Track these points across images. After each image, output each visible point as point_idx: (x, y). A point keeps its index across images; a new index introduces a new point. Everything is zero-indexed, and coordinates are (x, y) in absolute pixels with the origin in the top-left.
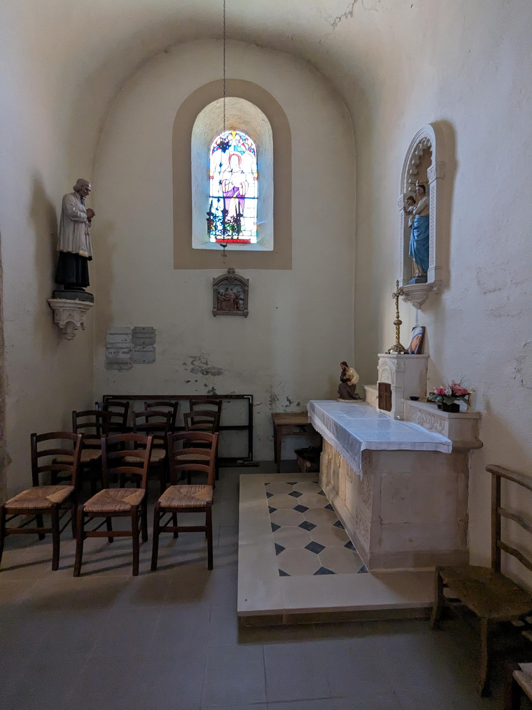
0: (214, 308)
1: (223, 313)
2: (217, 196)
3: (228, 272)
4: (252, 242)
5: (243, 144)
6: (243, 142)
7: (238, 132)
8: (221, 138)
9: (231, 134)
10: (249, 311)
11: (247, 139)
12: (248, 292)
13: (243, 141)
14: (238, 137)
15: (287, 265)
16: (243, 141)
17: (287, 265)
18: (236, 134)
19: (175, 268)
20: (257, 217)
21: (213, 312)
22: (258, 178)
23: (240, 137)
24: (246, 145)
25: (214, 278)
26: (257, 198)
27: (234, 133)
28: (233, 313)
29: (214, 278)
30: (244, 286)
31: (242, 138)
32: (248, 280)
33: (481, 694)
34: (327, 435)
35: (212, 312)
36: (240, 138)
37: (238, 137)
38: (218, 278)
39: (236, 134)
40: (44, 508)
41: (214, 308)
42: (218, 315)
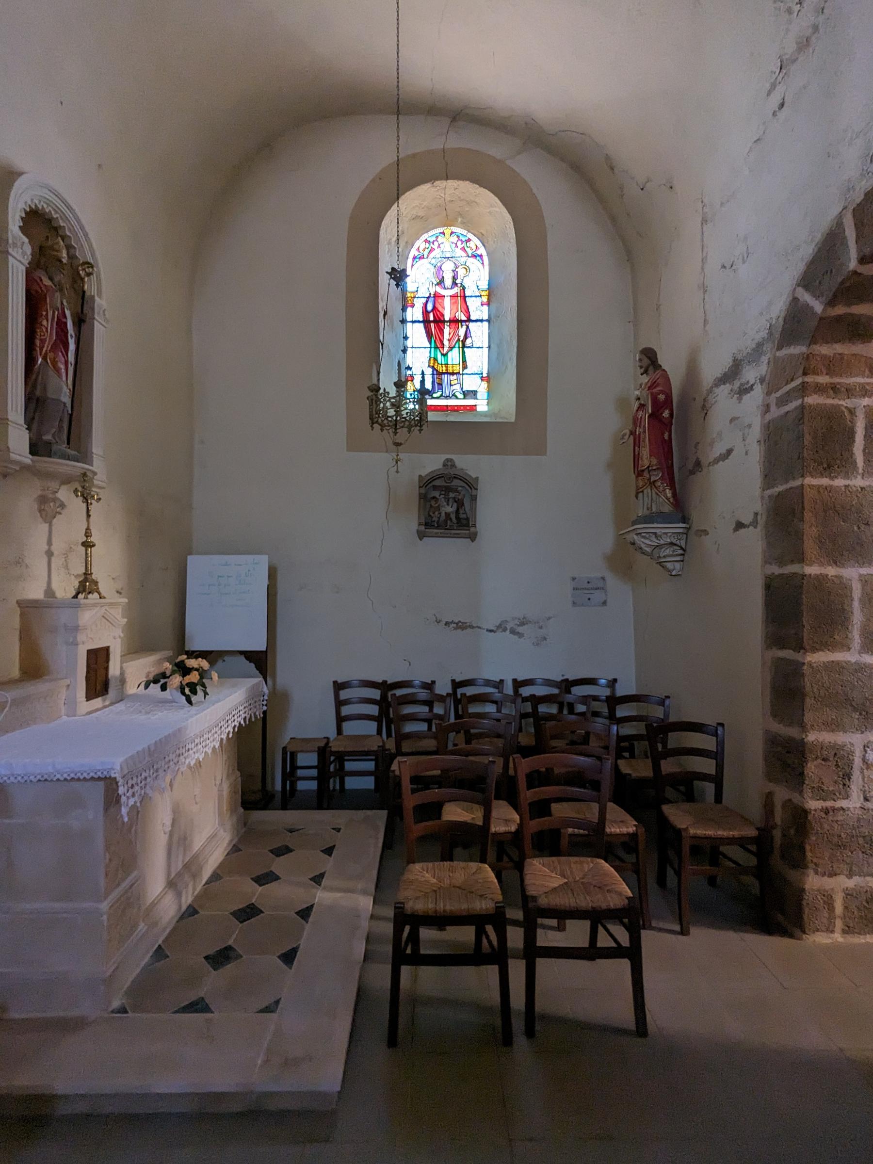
0: (419, 525)
1: (437, 533)
2: (379, 679)
3: (444, 465)
4: (479, 409)
5: (463, 249)
6: (463, 245)
7: (454, 229)
8: (426, 241)
9: (443, 233)
10: (478, 530)
11: (469, 240)
12: (476, 498)
13: (462, 244)
14: (454, 239)
15: (538, 447)
16: (462, 244)
17: (538, 447)
18: (452, 233)
19: (350, 448)
20: (489, 347)
21: (418, 531)
22: (488, 304)
23: (458, 237)
24: (468, 250)
25: (420, 476)
26: (488, 321)
27: (448, 231)
28: (451, 534)
29: (420, 476)
30: (471, 488)
31: (460, 238)
32: (477, 478)
33: (767, 331)
34: (609, 794)
35: (416, 531)
36: (457, 239)
37: (454, 239)
38: (427, 475)
39: (452, 233)
40: (124, 690)
41: (420, 524)
42: (427, 537)
